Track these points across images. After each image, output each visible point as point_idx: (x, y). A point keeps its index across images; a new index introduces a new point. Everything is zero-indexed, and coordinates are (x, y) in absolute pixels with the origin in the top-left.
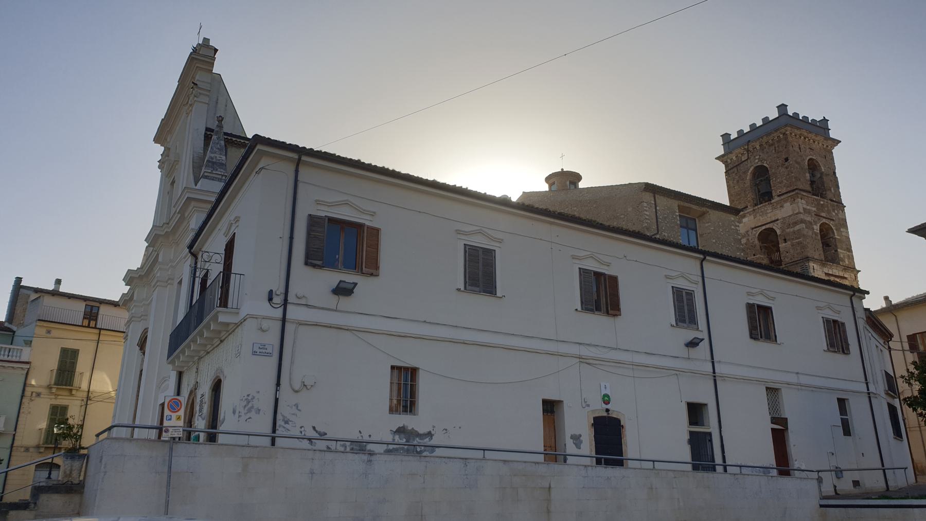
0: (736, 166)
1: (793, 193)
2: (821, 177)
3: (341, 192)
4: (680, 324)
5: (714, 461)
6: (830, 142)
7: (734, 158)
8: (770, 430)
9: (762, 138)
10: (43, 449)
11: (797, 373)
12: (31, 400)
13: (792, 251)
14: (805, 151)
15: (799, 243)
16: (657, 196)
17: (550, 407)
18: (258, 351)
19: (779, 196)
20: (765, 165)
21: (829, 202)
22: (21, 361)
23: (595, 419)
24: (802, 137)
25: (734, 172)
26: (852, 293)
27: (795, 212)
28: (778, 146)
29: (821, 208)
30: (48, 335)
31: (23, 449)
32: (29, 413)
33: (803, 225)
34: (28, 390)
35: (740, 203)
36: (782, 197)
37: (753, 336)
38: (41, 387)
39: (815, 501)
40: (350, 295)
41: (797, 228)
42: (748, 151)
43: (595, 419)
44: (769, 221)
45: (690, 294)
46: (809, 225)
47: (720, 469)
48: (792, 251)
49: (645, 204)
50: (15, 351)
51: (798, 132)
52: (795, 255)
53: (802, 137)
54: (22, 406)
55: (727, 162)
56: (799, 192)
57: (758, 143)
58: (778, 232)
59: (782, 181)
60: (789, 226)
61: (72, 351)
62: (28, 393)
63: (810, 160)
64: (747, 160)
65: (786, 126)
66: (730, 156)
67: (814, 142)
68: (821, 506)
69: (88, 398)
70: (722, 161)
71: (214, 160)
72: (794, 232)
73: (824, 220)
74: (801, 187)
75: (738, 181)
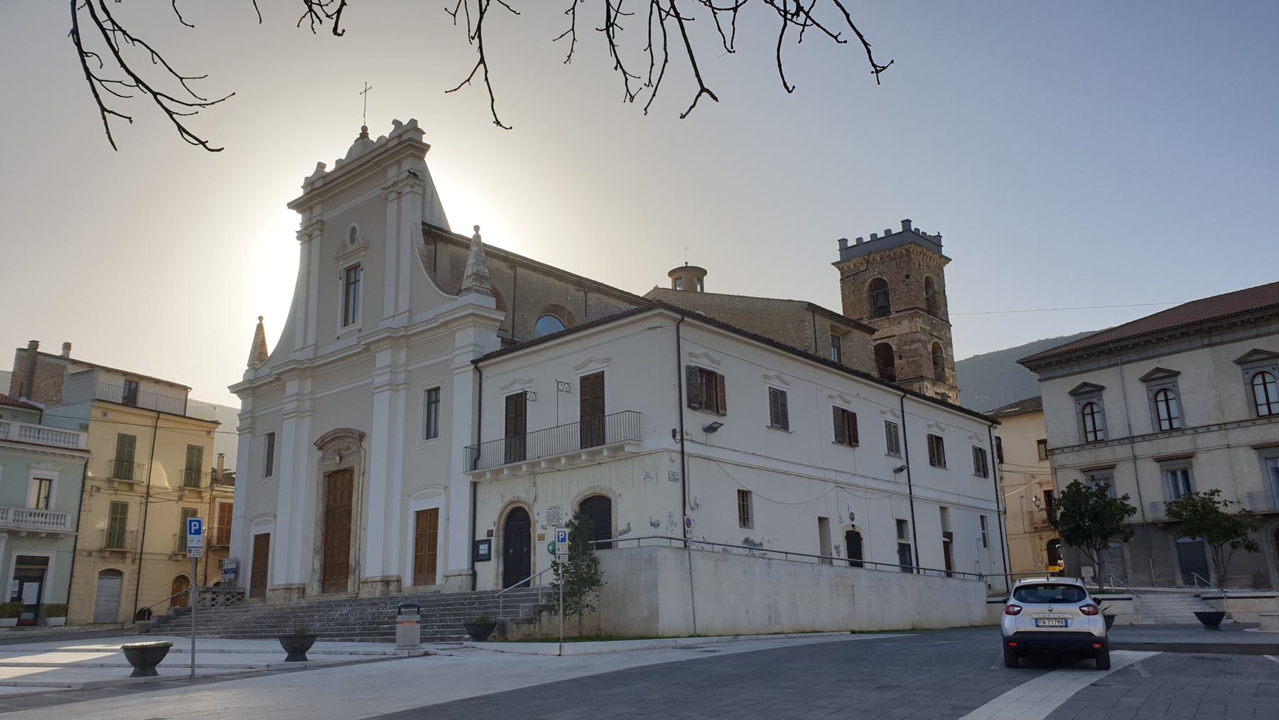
0: (854, 275)
1: (911, 312)
2: (933, 295)
3: (702, 346)
4: (890, 453)
5: (911, 565)
6: (943, 260)
7: (852, 266)
8: (942, 543)
9: (884, 251)
10: (108, 553)
11: (958, 495)
12: (92, 496)
13: (907, 368)
14: (923, 268)
15: (914, 361)
16: (87, 5)
17: (822, 521)
18: (672, 477)
19: (897, 312)
20: (885, 279)
21: (940, 321)
22: (78, 448)
23: (847, 532)
24: (922, 255)
25: (850, 281)
26: (990, 424)
27: (913, 331)
28: (900, 262)
29: (933, 326)
30: (104, 418)
31: (85, 554)
32: (91, 511)
33: (920, 345)
34: (88, 483)
35: (855, 313)
36: (901, 314)
37: (932, 464)
38: (101, 480)
39: (984, 599)
40: (714, 432)
41: (913, 346)
42: (868, 262)
43: (847, 532)
44: (885, 336)
45: (896, 427)
46: (925, 343)
47: (915, 571)
48: (907, 368)
49: (807, 324)
50: (71, 436)
51: (919, 250)
52: (910, 373)
53: (922, 255)
54: (83, 503)
55: (843, 269)
56: (918, 311)
57: (879, 255)
58: (894, 348)
59: (902, 298)
60: (905, 344)
61: (129, 438)
62: (87, 488)
63: (927, 277)
64: (865, 270)
65: (911, 243)
66: (848, 264)
67: (931, 259)
68: (988, 602)
69: (148, 495)
70: (839, 268)
71: (480, 273)
72: (911, 350)
73: (936, 340)
74: (919, 306)
75: (854, 291)
